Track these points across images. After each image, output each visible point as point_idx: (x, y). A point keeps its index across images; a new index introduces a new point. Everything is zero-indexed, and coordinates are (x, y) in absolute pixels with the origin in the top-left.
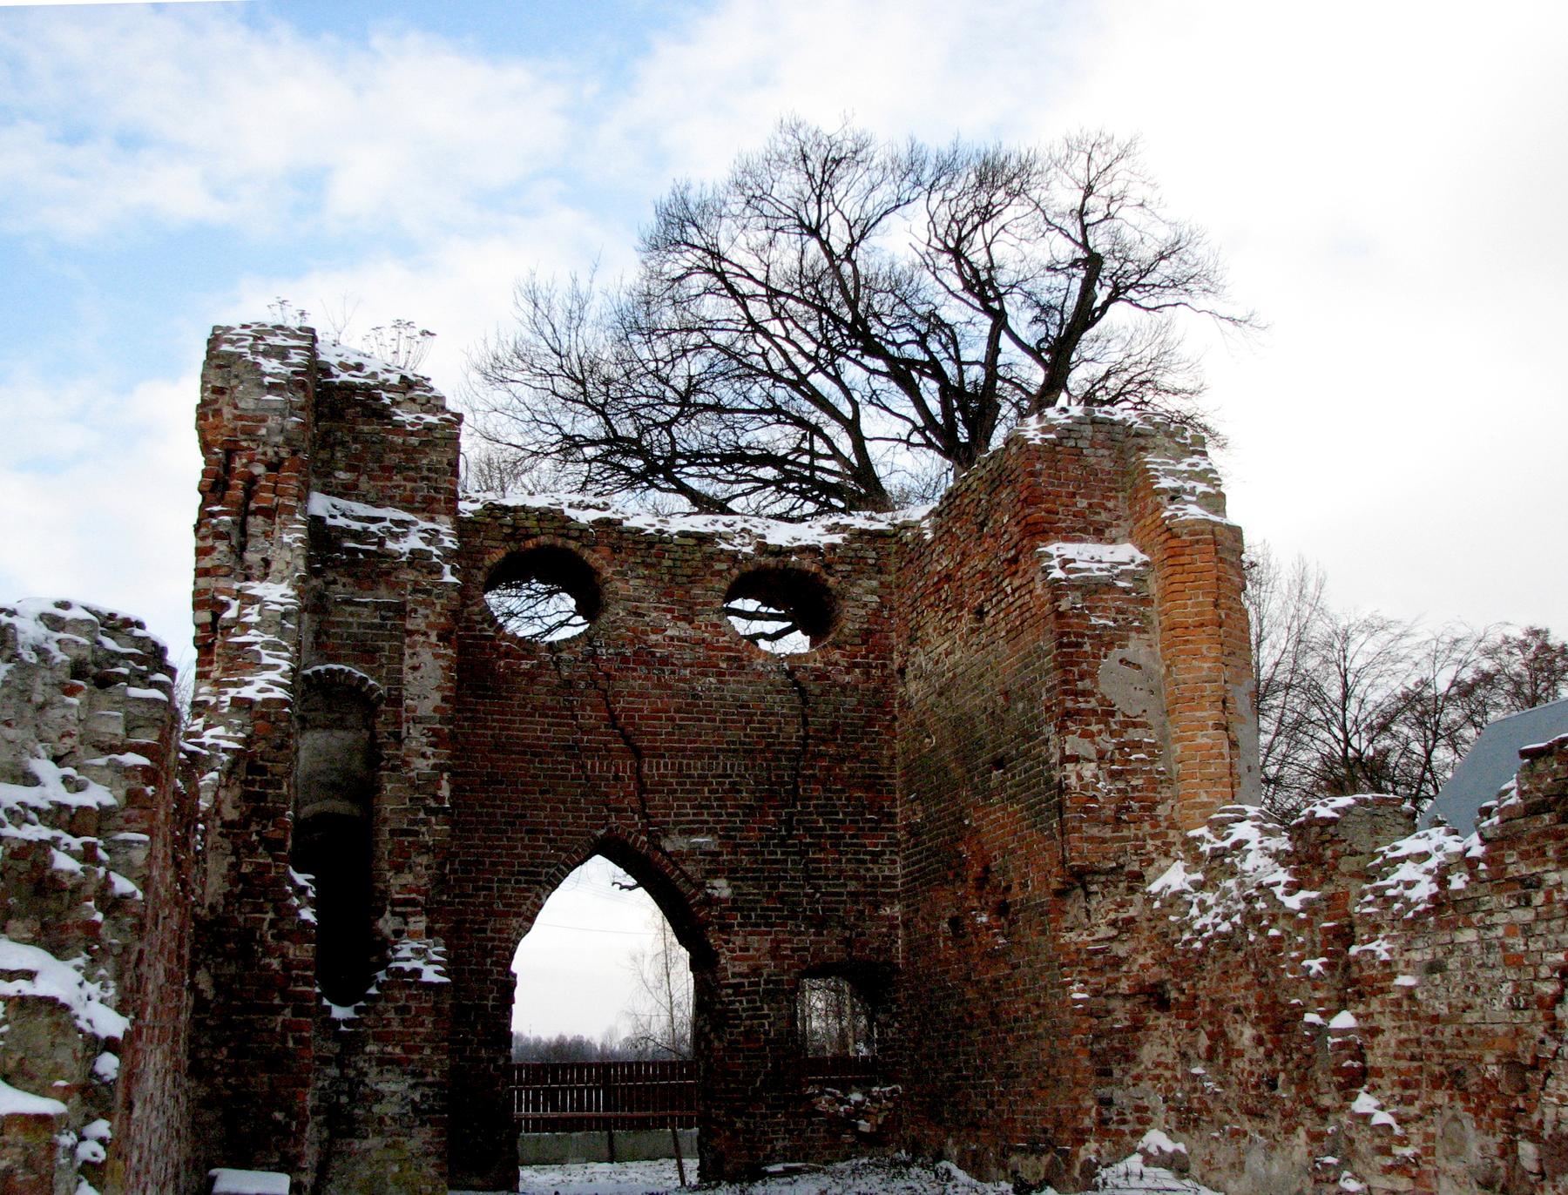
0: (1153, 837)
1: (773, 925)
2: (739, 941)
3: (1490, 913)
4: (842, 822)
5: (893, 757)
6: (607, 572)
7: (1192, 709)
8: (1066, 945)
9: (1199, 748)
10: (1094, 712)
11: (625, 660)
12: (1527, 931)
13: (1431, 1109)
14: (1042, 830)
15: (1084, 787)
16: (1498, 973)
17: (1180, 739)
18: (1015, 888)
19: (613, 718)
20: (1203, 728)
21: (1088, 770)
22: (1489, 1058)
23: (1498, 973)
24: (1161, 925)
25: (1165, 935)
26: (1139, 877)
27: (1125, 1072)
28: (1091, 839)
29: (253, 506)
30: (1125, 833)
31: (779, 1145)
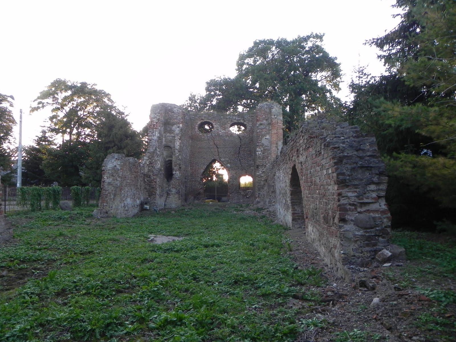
21: (260, 153)
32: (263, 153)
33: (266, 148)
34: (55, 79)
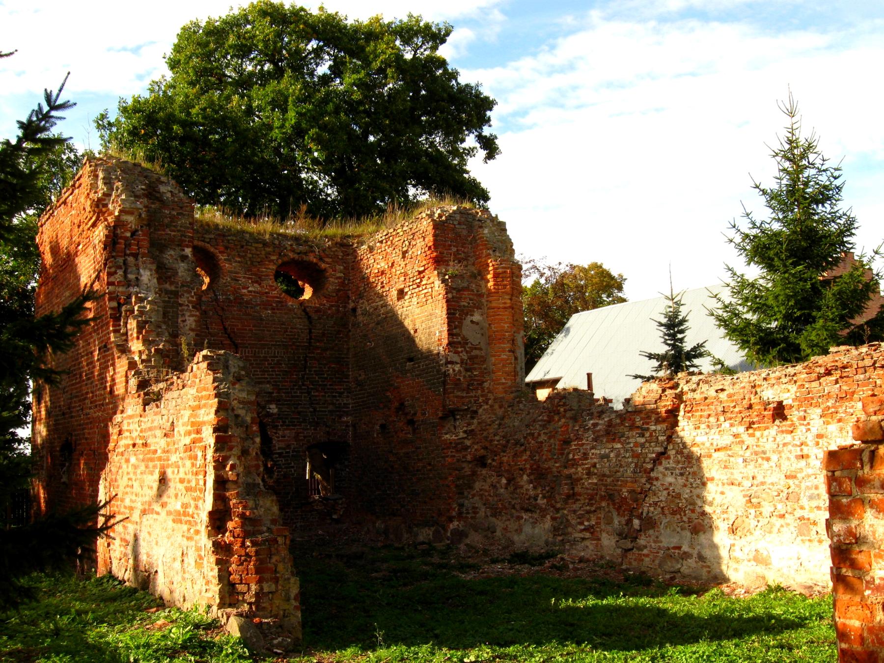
0: (482, 396)
1: (295, 426)
2: (281, 433)
3: (628, 438)
4: (326, 378)
5: (348, 349)
6: (222, 257)
7: (500, 343)
8: (446, 440)
9: (502, 360)
10: (459, 343)
11: (230, 301)
12: (642, 446)
13: (600, 508)
14: (435, 391)
15: (455, 375)
16: (630, 460)
17: (494, 356)
18: (419, 414)
19: (225, 329)
20: (504, 351)
21: (457, 368)
22: (624, 490)
23: (630, 460)
24: (485, 434)
25: (487, 437)
26: (476, 412)
27: (469, 493)
28: (457, 397)
29: (128, 252)
30: (471, 394)
31: (298, 525)
32: (467, 370)
33: (475, 353)
34: (298, 6)
